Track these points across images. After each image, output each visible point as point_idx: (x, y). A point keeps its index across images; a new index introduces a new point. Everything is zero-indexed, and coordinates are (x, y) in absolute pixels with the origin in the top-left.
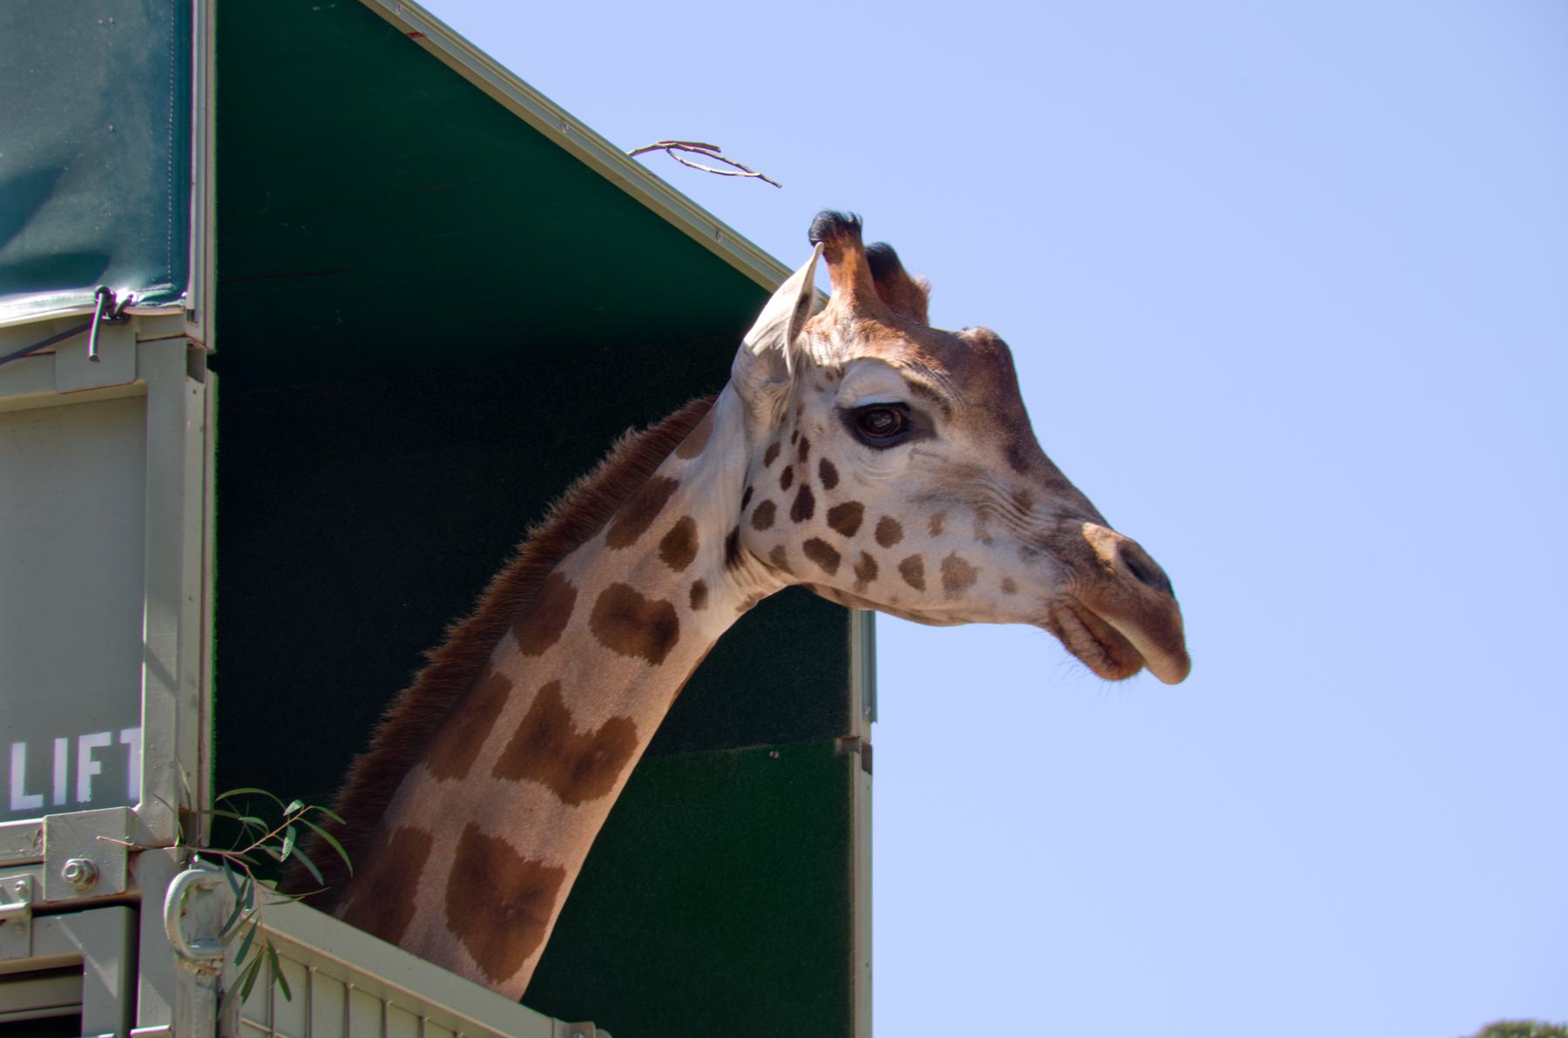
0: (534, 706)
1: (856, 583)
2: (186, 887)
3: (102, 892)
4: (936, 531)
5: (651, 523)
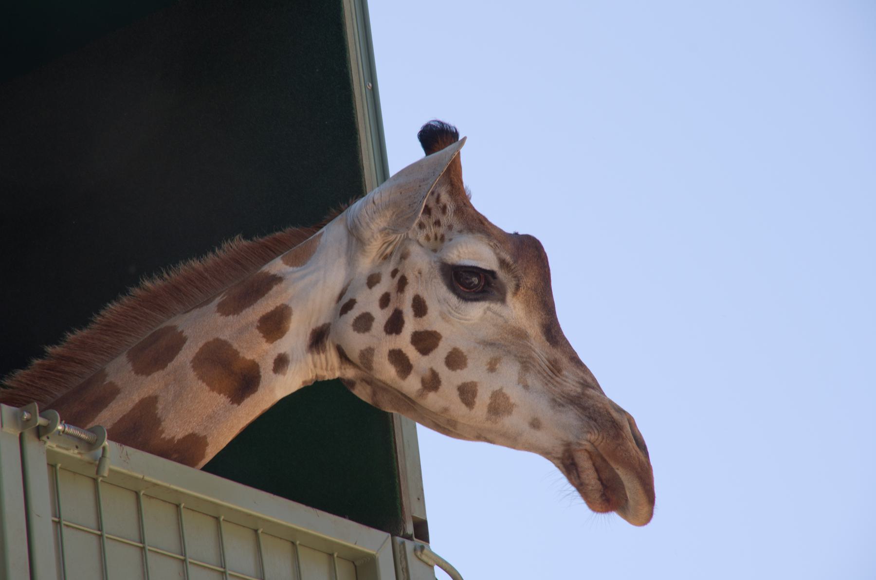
0: (134, 409)
1: (420, 390)
4: (492, 368)
5: (255, 302)
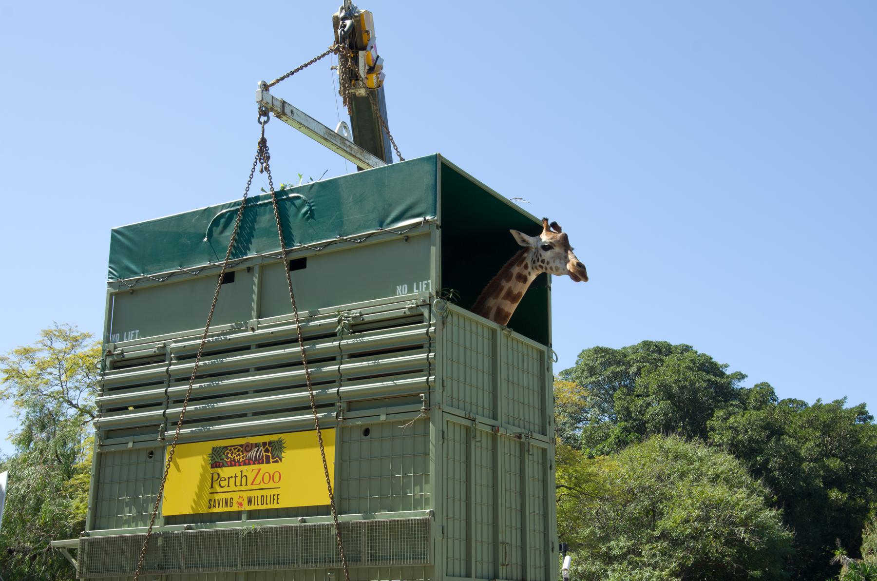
2: (437, 302)
3: (426, 303)
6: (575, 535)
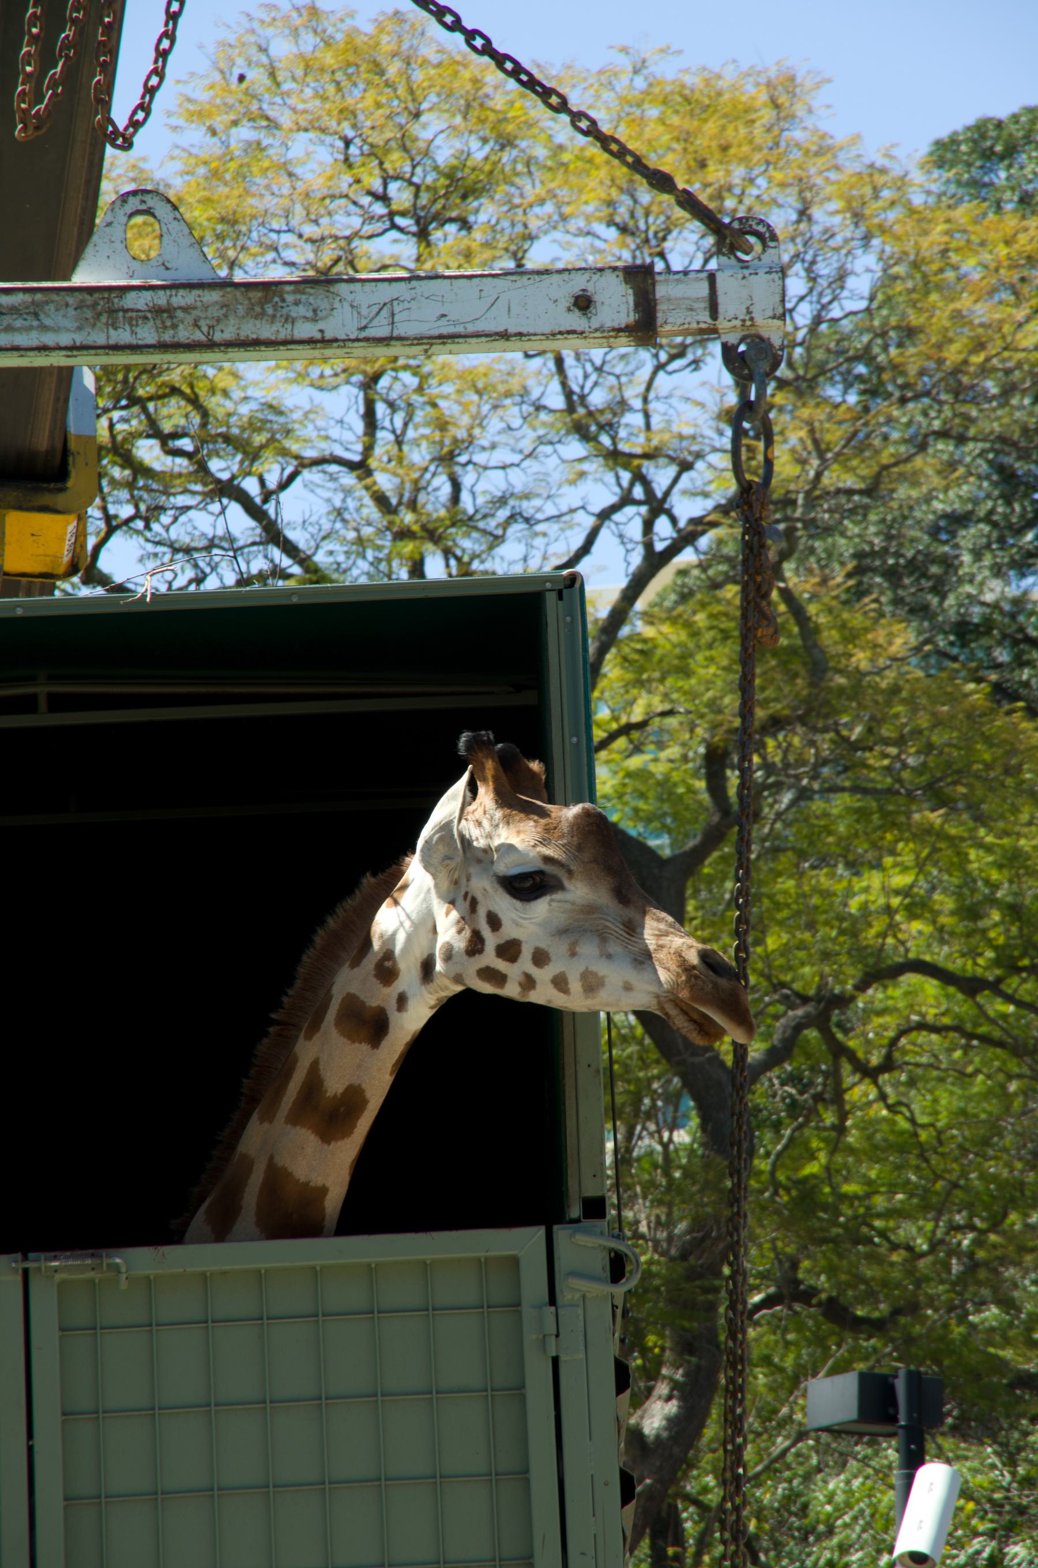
6: (992, 1314)
